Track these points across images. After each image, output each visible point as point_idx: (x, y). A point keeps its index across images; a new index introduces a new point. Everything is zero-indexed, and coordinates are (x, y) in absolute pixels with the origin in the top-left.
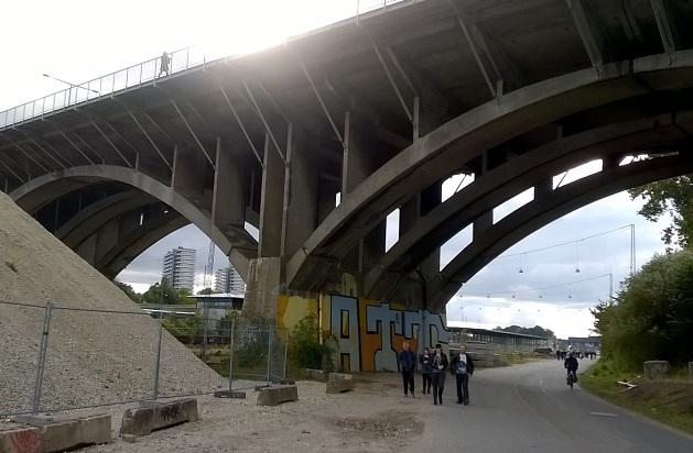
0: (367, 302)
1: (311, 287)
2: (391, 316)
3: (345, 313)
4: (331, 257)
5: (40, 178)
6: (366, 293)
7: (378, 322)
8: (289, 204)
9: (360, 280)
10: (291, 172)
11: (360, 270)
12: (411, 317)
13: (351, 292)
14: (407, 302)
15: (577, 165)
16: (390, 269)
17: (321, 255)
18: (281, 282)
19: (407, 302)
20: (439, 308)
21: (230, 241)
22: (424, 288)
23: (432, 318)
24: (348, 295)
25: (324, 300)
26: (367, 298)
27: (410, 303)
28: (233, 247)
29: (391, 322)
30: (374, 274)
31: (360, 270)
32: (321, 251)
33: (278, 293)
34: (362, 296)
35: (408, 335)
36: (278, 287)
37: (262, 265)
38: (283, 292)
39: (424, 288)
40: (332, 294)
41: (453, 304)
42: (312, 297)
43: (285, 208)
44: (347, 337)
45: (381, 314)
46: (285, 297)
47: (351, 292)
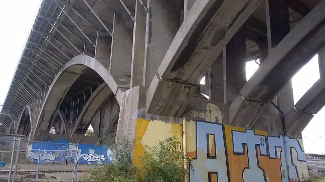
0: (233, 128)
1: (173, 112)
2: (257, 140)
3: (211, 138)
4: (186, 82)
5: (97, 89)
6: (231, 121)
7: (244, 144)
8: (150, 41)
9: (225, 110)
10: (150, 16)
11: (225, 102)
12: (274, 142)
13: (216, 118)
14: (269, 129)
15: (304, 128)
16: (251, 98)
17: (176, 80)
18: (139, 107)
19: (269, 129)
20: (297, 134)
21: (117, 84)
22: (283, 119)
23: (291, 142)
24: (214, 121)
25: (189, 126)
26: (233, 124)
27: (272, 130)
28: (118, 87)
29: (257, 145)
30: (236, 104)
31: (225, 102)
32: (174, 75)
33: (136, 117)
34: (227, 122)
35: (272, 155)
36: (136, 112)
37: (129, 96)
38: (142, 116)
39: (283, 119)
40: (197, 120)
41: (308, 132)
42: (175, 121)
43: (146, 45)
44: (214, 157)
45: (246, 138)
46: (144, 121)
47: (216, 118)
